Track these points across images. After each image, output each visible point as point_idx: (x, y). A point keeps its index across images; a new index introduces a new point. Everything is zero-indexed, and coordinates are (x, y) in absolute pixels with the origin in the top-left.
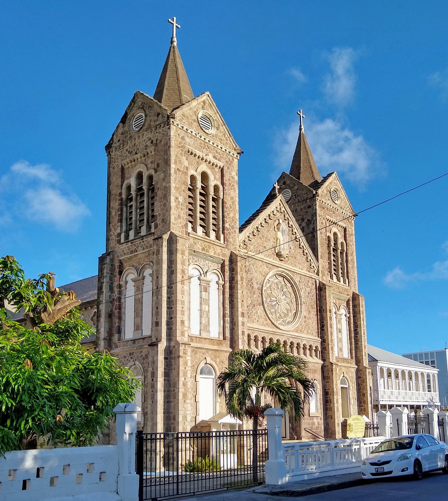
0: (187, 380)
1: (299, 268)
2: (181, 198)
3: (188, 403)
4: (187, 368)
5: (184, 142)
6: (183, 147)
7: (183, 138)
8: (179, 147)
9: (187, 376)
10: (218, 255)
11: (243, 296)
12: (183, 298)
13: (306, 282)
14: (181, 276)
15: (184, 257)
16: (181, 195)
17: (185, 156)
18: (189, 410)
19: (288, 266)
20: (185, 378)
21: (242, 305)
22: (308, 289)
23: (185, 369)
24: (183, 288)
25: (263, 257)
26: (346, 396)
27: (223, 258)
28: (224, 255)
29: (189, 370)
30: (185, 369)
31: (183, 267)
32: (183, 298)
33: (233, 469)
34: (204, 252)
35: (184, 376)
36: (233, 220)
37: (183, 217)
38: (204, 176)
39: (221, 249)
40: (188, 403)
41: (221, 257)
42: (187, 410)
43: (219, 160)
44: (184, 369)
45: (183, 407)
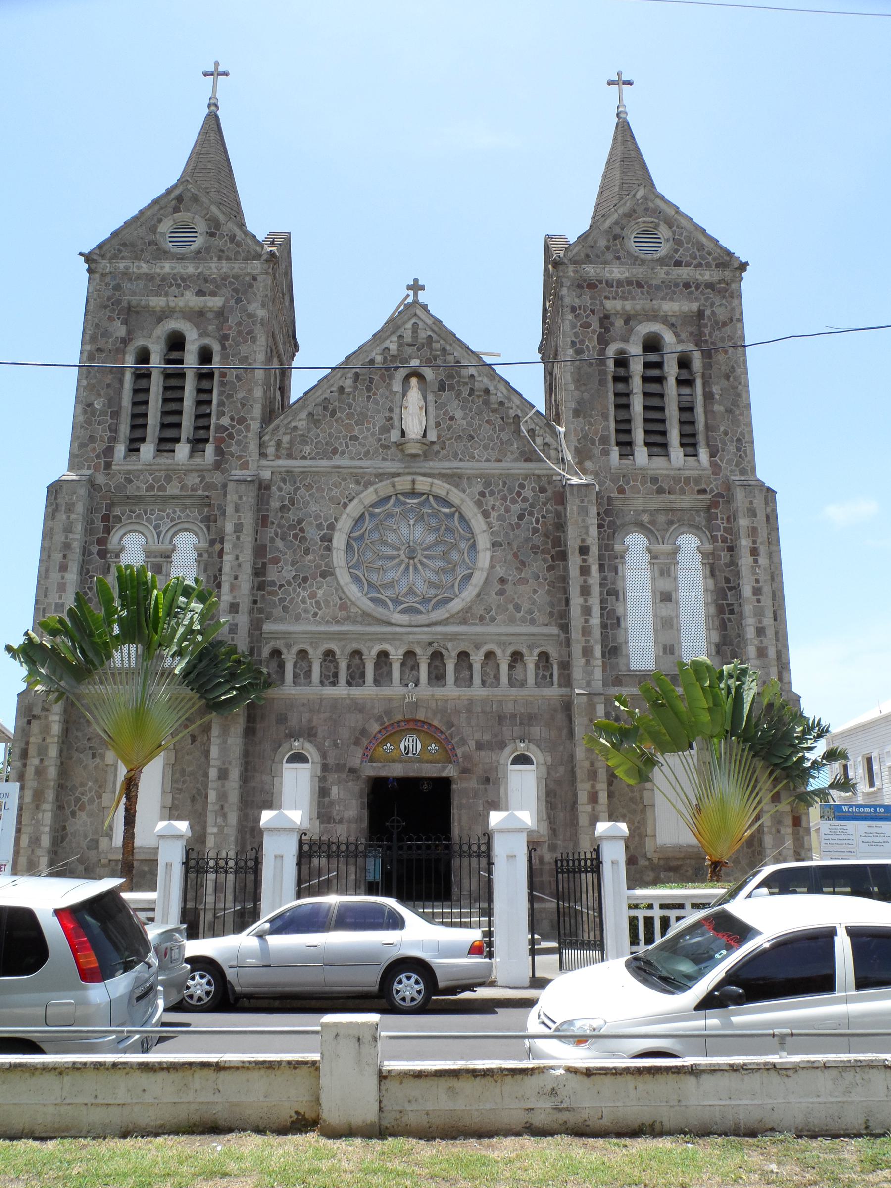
0: (46, 763)
1: (488, 461)
2: (98, 404)
3: (44, 811)
4: (48, 740)
5: (117, 293)
6: (119, 302)
7: (117, 287)
8: (106, 307)
9: (46, 755)
10: (192, 490)
11: (239, 565)
12: (60, 597)
13: (511, 490)
14: (61, 555)
15: (73, 516)
16: (99, 395)
17: (119, 319)
18: (45, 826)
19: (447, 464)
20: (42, 760)
21: (232, 588)
22: (516, 508)
23: (44, 740)
24: (63, 578)
25: (509, 465)
26: (122, 1083)
27: (207, 493)
28: (209, 486)
29: (53, 743)
30: (44, 740)
31: (67, 537)
32: (60, 597)
33: (341, 859)
34: (152, 493)
35: (39, 755)
36: (243, 405)
37: (101, 436)
38: (652, 345)
39: (199, 476)
40: (44, 811)
41: (200, 492)
42: (42, 825)
43: (213, 294)
44: (40, 740)
45: (33, 819)
